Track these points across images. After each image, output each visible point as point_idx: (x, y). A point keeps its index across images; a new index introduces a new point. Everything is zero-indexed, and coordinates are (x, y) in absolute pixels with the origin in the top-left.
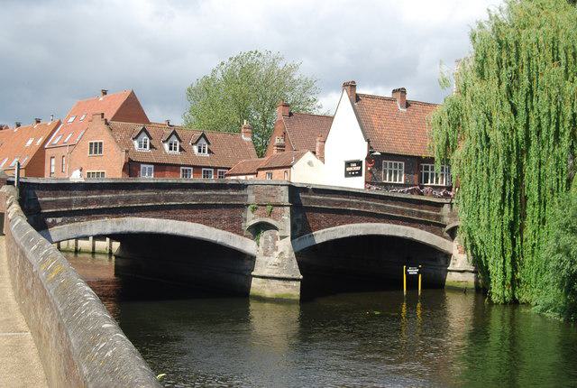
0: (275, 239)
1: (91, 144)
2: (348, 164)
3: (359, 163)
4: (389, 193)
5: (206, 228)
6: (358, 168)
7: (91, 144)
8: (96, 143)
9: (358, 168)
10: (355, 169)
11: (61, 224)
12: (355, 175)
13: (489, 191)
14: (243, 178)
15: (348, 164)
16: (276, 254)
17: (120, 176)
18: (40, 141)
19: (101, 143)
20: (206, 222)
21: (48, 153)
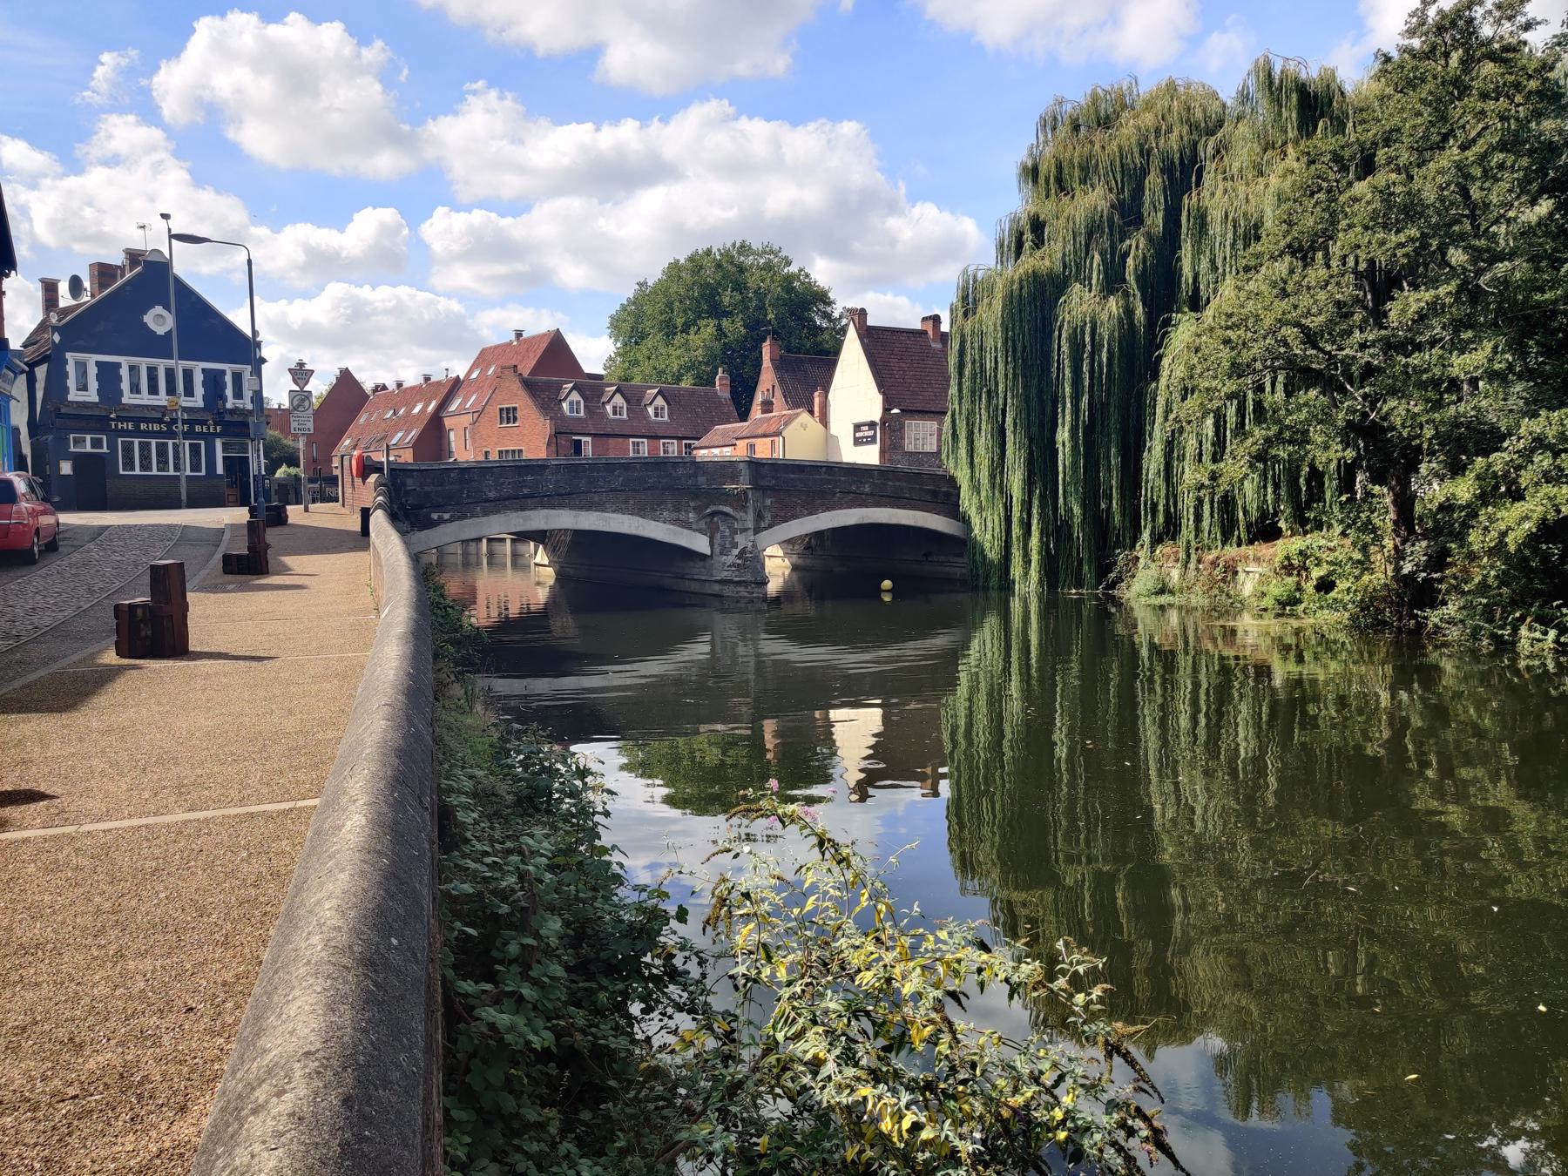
0: (734, 532)
1: (501, 410)
2: (857, 427)
3: (872, 425)
4: (1016, 531)
5: (864, 510)
6: (871, 433)
7: (501, 410)
8: (508, 409)
9: (871, 433)
10: (866, 434)
11: (450, 521)
12: (868, 443)
13: (63, 1101)
14: (716, 451)
15: (857, 427)
16: (736, 552)
17: (543, 455)
18: (431, 408)
19: (515, 409)
20: (641, 511)
21: (448, 422)
